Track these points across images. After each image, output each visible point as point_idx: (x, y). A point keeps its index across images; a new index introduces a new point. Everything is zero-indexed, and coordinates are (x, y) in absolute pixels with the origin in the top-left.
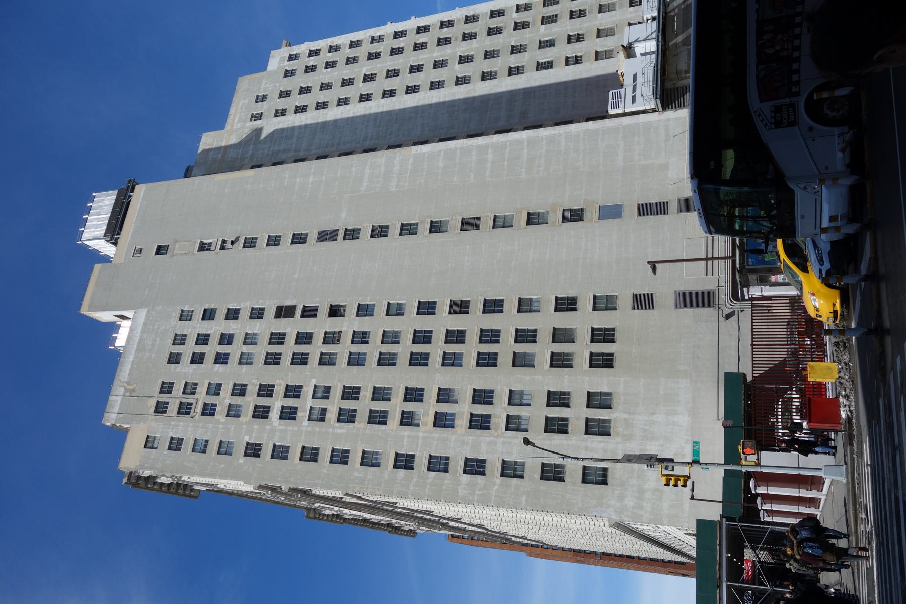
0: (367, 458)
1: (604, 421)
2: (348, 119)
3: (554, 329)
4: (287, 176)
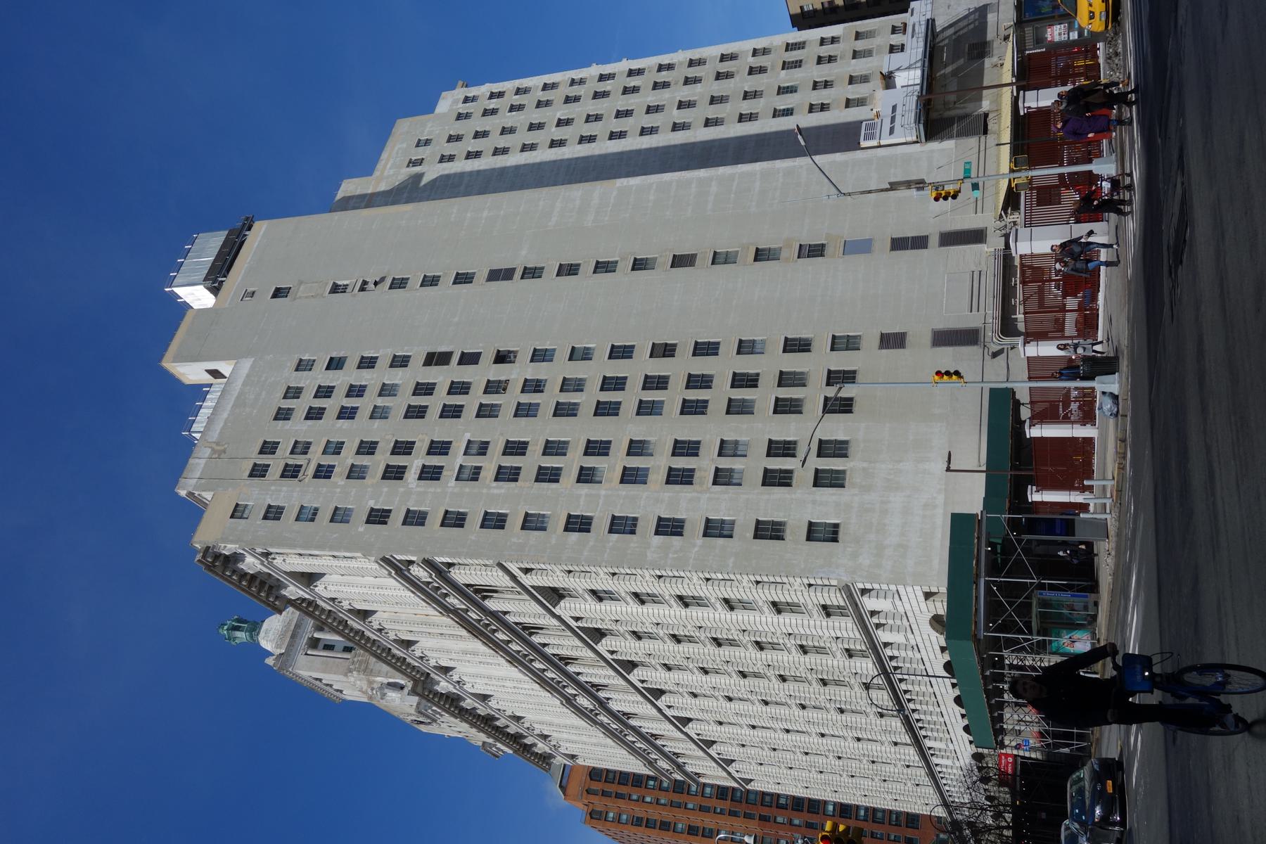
0: (531, 521)
1: (838, 472)
2: (534, 164)
3: (781, 373)
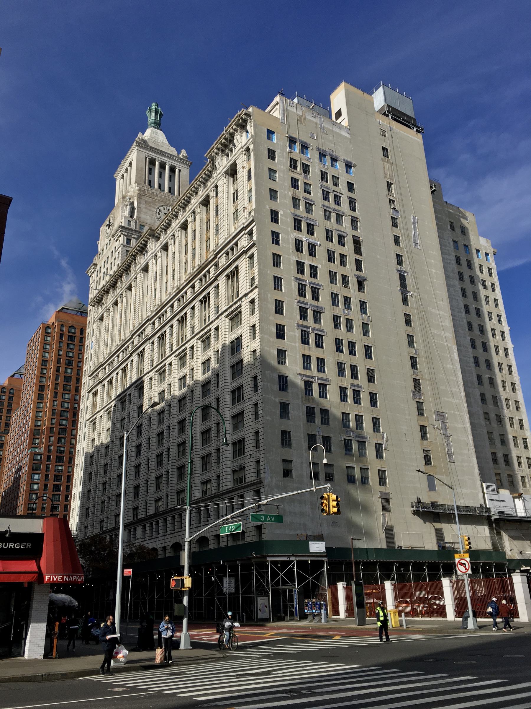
4: (434, 253)
